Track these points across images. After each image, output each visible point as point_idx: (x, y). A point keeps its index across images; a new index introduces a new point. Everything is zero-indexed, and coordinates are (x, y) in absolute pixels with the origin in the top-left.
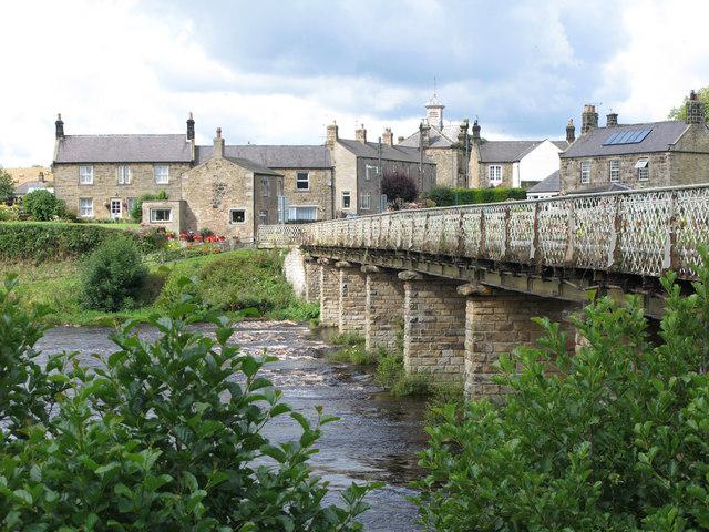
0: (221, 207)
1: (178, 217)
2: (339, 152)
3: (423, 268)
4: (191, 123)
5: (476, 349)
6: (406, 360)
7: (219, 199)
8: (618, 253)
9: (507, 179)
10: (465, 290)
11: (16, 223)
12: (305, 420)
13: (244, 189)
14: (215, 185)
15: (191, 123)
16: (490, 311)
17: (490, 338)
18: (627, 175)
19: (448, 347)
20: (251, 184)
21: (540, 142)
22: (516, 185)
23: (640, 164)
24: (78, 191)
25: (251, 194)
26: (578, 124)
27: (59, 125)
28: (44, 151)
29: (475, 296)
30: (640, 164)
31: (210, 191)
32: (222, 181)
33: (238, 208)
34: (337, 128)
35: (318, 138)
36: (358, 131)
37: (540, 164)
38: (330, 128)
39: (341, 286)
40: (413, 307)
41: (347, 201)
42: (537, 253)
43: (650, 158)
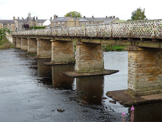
2: (16, 21)
3: (40, 38)
5: (54, 49)
6: (38, 52)
8: (86, 34)
9: (42, 25)
10: (51, 41)
12: (124, 34)
16: (56, 44)
17: (56, 48)
18: (61, 25)
19: (44, 50)
21: (47, 20)
22: (43, 26)
23: (63, 23)
29: (53, 41)
30: (63, 23)
35: (12, 19)
36: (18, 18)
37: (47, 23)
39: (22, 41)
40: (39, 44)
41: (17, 29)
42: (68, 34)
43: (64, 22)
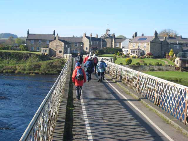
0: (57, 50)
1: (150, 76)
4: (54, 32)
7: (57, 48)
11: (12, 90)
13: (62, 46)
14: (56, 45)
15: (54, 32)
20: (63, 45)
24: (31, 45)
25: (63, 47)
26: (134, 35)
27: (28, 31)
28: (25, 35)
31: (55, 46)
32: (58, 44)
33: (60, 50)
34: (86, 34)
38: (84, 34)
41: (87, 49)
